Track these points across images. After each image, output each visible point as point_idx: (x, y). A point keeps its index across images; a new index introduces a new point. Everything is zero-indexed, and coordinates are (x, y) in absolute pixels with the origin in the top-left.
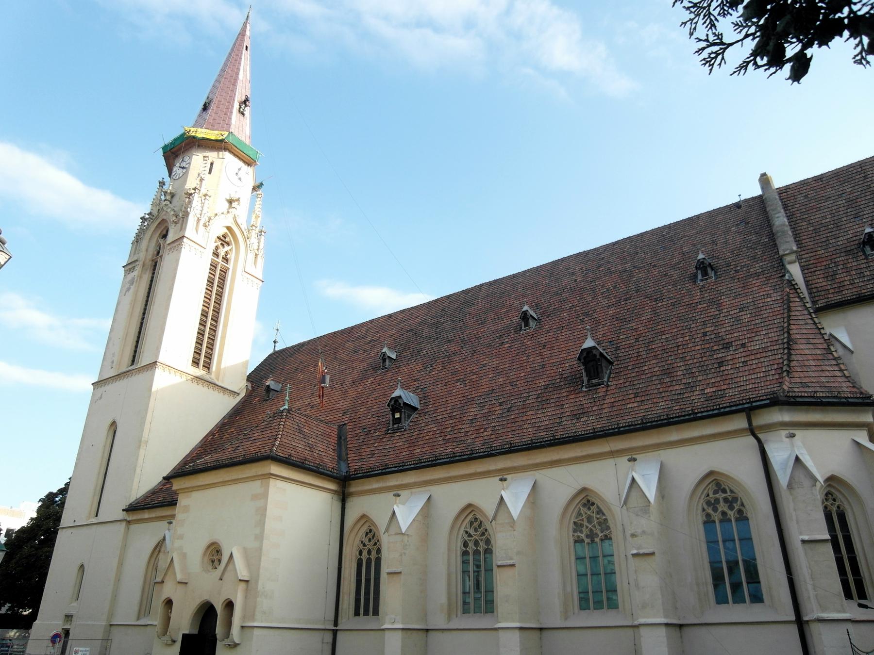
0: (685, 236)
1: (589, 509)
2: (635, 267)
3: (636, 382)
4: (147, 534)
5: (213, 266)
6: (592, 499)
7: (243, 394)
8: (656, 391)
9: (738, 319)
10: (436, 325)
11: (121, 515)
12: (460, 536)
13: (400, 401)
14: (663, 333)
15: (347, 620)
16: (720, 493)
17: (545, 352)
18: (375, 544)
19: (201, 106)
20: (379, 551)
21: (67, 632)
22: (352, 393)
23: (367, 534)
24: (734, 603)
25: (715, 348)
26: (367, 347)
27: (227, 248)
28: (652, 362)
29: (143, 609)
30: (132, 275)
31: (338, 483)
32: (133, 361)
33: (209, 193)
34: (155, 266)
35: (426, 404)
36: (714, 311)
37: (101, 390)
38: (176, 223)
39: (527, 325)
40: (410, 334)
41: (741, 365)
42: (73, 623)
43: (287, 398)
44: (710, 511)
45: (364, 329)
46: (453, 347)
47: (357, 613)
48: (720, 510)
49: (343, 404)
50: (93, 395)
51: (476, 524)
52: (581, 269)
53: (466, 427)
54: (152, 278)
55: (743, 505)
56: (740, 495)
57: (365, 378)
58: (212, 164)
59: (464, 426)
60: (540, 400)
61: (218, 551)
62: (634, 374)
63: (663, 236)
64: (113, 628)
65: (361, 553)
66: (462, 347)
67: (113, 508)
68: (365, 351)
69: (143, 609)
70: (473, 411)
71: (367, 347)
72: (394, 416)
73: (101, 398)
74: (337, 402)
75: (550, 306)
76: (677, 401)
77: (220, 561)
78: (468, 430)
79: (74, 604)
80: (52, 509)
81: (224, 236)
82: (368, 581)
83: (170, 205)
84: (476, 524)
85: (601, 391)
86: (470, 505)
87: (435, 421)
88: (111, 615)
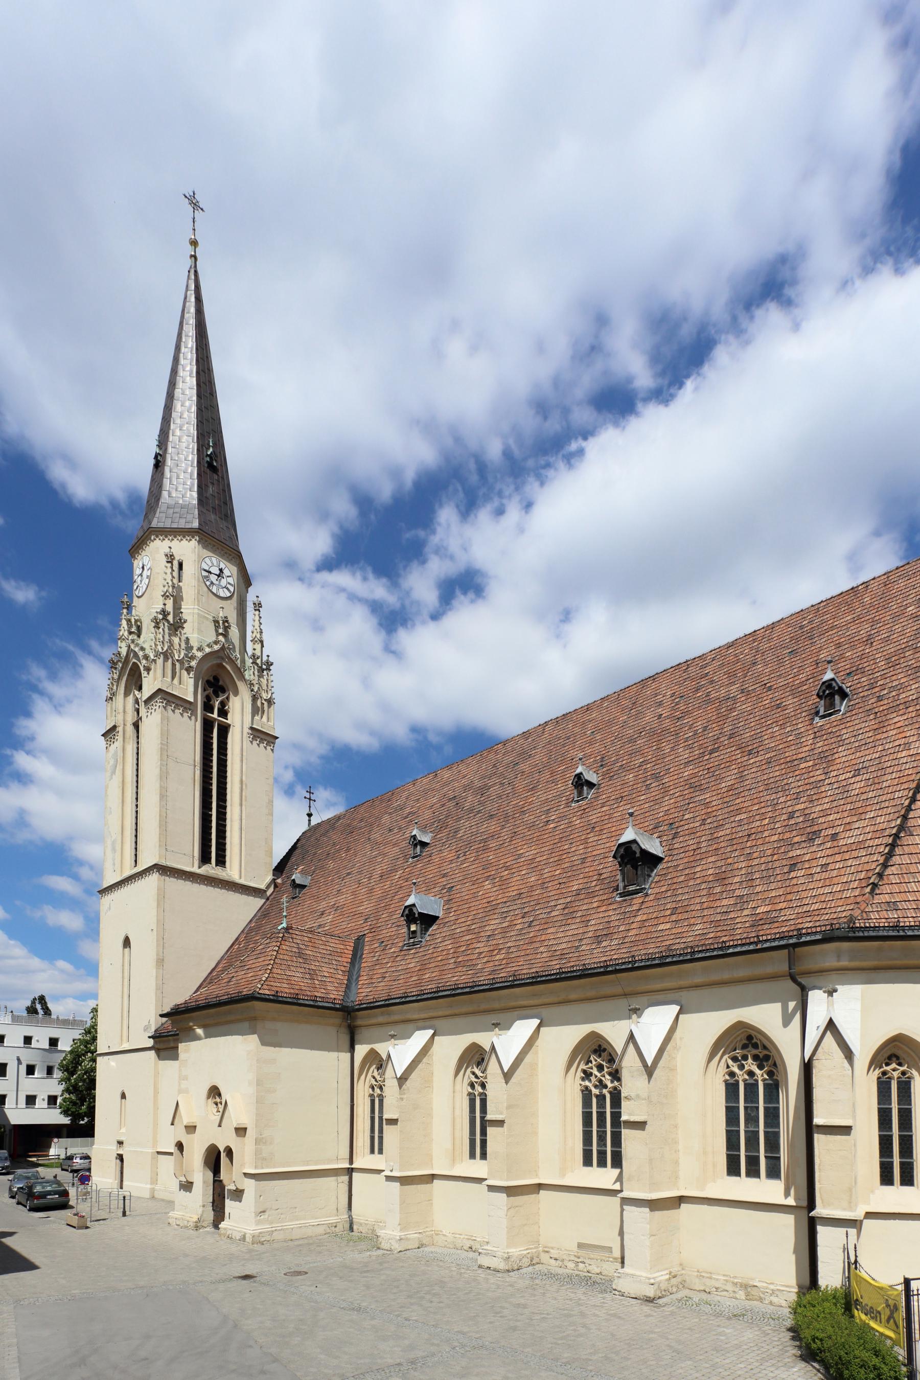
0: (832, 628)
1: (600, 1056)
2: (742, 691)
3: (680, 891)
6: (604, 1046)
8: (698, 907)
9: (845, 789)
10: (482, 790)
14: (739, 811)
16: (750, 1048)
17: (592, 838)
22: (378, 892)
25: (796, 839)
26: (403, 823)
28: (710, 859)
36: (818, 775)
40: (451, 804)
41: (818, 870)
44: (736, 1069)
46: (493, 826)
48: (747, 1068)
52: (673, 695)
53: (481, 947)
55: (775, 1065)
56: (774, 1053)
60: (566, 911)
62: (682, 878)
63: (801, 627)
66: (503, 827)
70: (494, 923)
72: (409, 929)
73: (110, 908)
76: (717, 924)
85: (638, 899)
87: (452, 936)
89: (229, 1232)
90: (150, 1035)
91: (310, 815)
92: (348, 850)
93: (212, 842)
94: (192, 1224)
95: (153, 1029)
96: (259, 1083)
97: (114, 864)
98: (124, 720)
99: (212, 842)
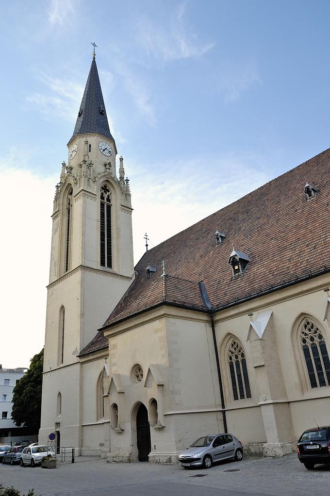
4: (94, 369)
5: (102, 205)
7: (134, 278)
11: (77, 360)
12: (299, 336)
13: (236, 258)
15: (231, 404)
18: (240, 351)
19: (78, 115)
20: (243, 355)
21: (58, 433)
22: (202, 262)
23: (232, 345)
24: (320, 386)
26: (204, 235)
27: (108, 193)
29: (99, 414)
30: (57, 220)
31: (208, 315)
32: (67, 269)
33: (92, 162)
34: (69, 212)
35: (254, 257)
37: (51, 289)
38: (76, 184)
39: (310, 195)
40: (231, 221)
42: (61, 428)
43: (164, 269)
45: (200, 226)
46: (262, 221)
47: (236, 398)
49: (197, 270)
50: (48, 293)
51: (309, 326)
54: (69, 219)
57: (208, 252)
58: (90, 146)
59: (285, 264)
61: (140, 370)
64: (83, 427)
65: (231, 358)
66: (268, 220)
67: (71, 357)
68: (203, 237)
69: (99, 414)
71: (204, 235)
72: (234, 268)
73: (52, 294)
74: (193, 270)
75: (324, 181)
77: (142, 376)
78: (288, 266)
79: (60, 416)
80: (38, 360)
81: (105, 186)
82: (239, 376)
83: (71, 175)
84: (309, 326)
86: (303, 314)
88: (81, 420)
89: (157, 458)
90: (78, 355)
91: (147, 245)
92: (175, 253)
93: (106, 258)
94: (126, 459)
95: (79, 352)
96: (170, 355)
97: (55, 272)
98: (63, 208)
99: (106, 258)
